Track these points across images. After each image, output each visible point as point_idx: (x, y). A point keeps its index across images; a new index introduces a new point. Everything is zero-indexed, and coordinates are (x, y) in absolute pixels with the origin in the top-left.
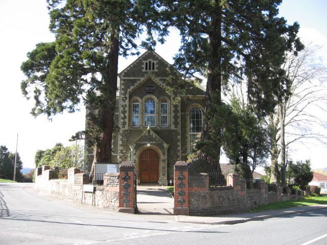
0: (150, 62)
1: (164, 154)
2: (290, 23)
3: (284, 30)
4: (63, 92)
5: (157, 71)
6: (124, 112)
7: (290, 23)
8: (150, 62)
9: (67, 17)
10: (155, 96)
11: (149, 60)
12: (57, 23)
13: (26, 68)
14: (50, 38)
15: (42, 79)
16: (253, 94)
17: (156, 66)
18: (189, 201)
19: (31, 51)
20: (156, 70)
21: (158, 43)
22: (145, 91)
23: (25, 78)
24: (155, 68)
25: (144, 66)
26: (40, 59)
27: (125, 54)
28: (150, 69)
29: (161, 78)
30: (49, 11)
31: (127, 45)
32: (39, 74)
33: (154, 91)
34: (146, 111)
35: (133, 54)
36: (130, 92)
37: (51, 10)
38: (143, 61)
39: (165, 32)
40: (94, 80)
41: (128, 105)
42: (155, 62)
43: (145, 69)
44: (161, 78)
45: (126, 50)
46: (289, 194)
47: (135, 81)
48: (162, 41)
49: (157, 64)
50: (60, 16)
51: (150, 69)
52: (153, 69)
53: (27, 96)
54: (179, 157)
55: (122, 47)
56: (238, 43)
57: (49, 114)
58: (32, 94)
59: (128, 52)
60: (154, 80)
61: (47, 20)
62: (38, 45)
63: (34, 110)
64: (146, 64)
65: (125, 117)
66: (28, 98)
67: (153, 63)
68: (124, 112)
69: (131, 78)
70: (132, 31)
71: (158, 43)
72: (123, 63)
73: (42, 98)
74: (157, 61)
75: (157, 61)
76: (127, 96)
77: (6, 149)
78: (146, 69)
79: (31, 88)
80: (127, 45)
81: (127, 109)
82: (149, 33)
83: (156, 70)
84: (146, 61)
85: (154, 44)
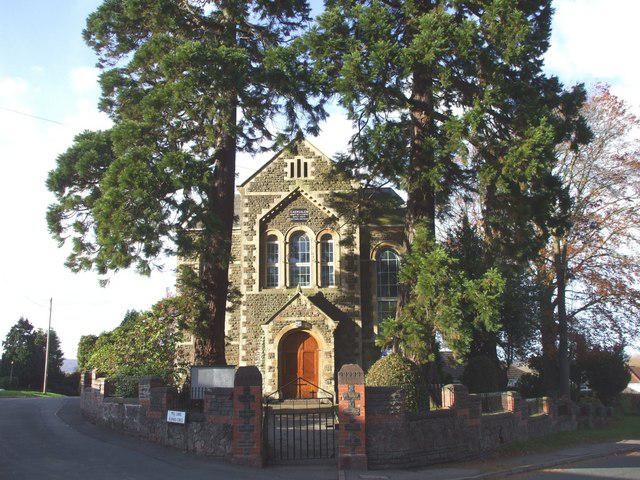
0: (299, 161)
1: (328, 340)
2: (568, 86)
3: (553, 102)
4: (122, 238)
5: (313, 178)
6: (249, 259)
7: (568, 86)
8: (299, 161)
9: (134, 83)
10: (311, 226)
11: (297, 157)
12: (115, 98)
13: (58, 182)
14: (104, 123)
15: (89, 203)
16: (496, 226)
17: (311, 169)
18: (367, 440)
19: (63, 151)
20: (310, 177)
21: (309, 137)
22: (291, 217)
23: (52, 199)
24: (309, 173)
25: (288, 169)
26: (80, 167)
27: (249, 147)
28: (299, 175)
29: (321, 192)
30: (100, 72)
31: (251, 131)
32: (86, 193)
33: (307, 217)
34: (297, 257)
35: (264, 149)
36: (261, 220)
37: (108, 69)
38: (285, 161)
39: (320, 112)
40: (187, 204)
41: (257, 246)
42: (310, 162)
43: (289, 174)
44: (321, 192)
45: (249, 143)
46: (574, 417)
47: (270, 199)
48: (315, 131)
49: (314, 164)
50: (120, 82)
51: (299, 175)
52: (306, 175)
53: (62, 235)
54: (358, 347)
55: (244, 136)
56: (403, 212)
57: (102, 270)
58: (70, 234)
59: (255, 146)
60: (307, 197)
61: (97, 92)
62: (77, 139)
63: (73, 257)
64: (292, 164)
65: (251, 268)
66: (62, 240)
67: (306, 164)
68: (249, 259)
69: (263, 193)
70: (259, 110)
71: (309, 137)
72: (246, 165)
73: (90, 237)
74: (313, 160)
75: (313, 160)
76: (257, 228)
77: (31, 327)
78: (292, 176)
79: (70, 219)
80: (251, 131)
81: (256, 253)
82: (292, 116)
83: (310, 177)
84: (292, 161)
85: (300, 137)
